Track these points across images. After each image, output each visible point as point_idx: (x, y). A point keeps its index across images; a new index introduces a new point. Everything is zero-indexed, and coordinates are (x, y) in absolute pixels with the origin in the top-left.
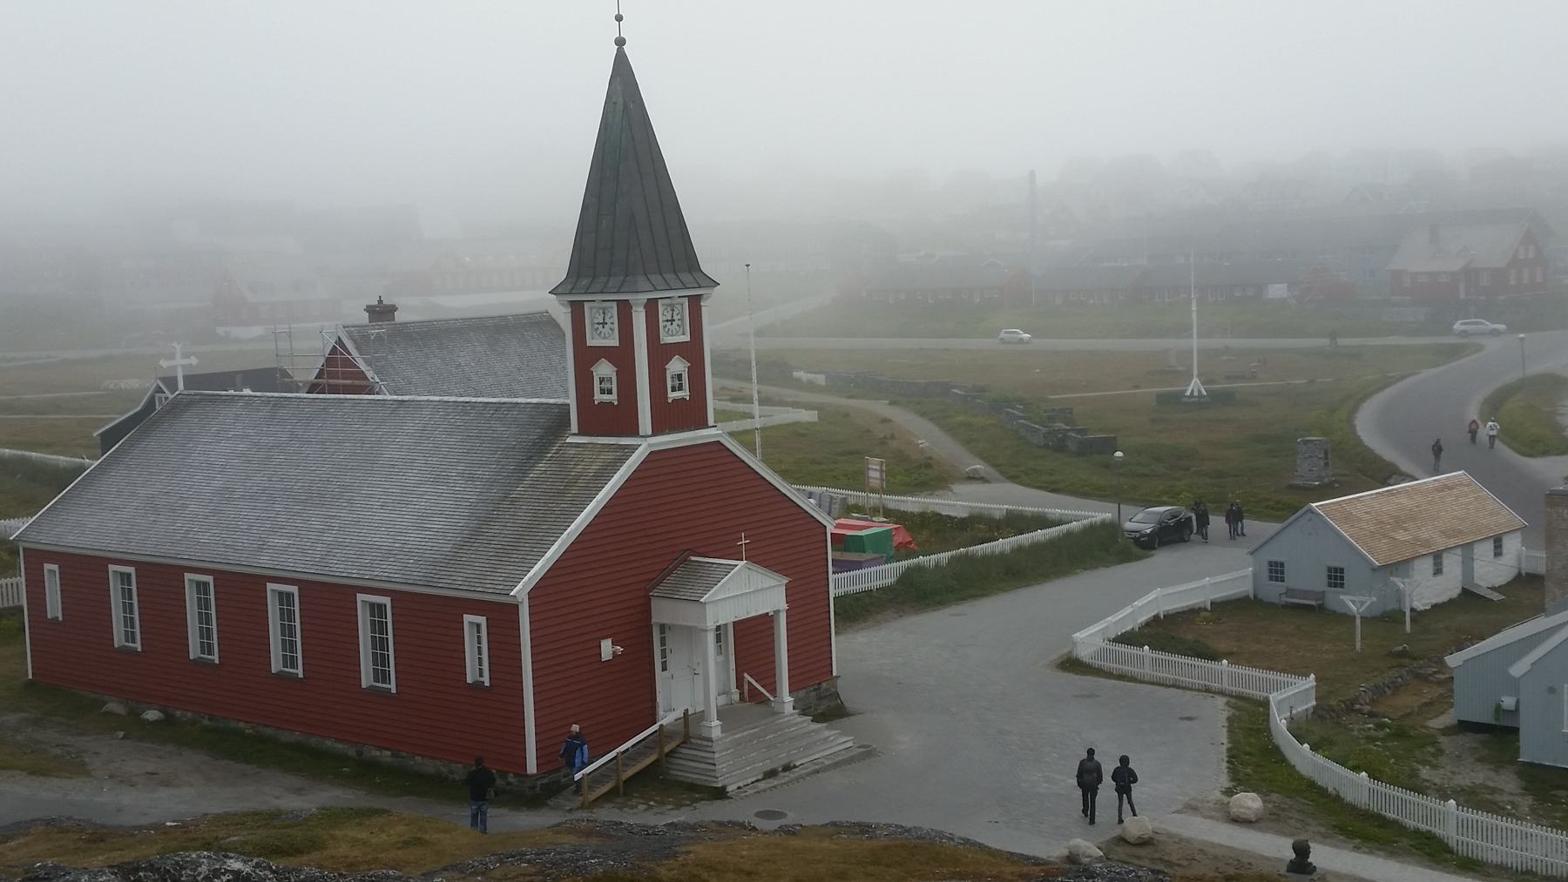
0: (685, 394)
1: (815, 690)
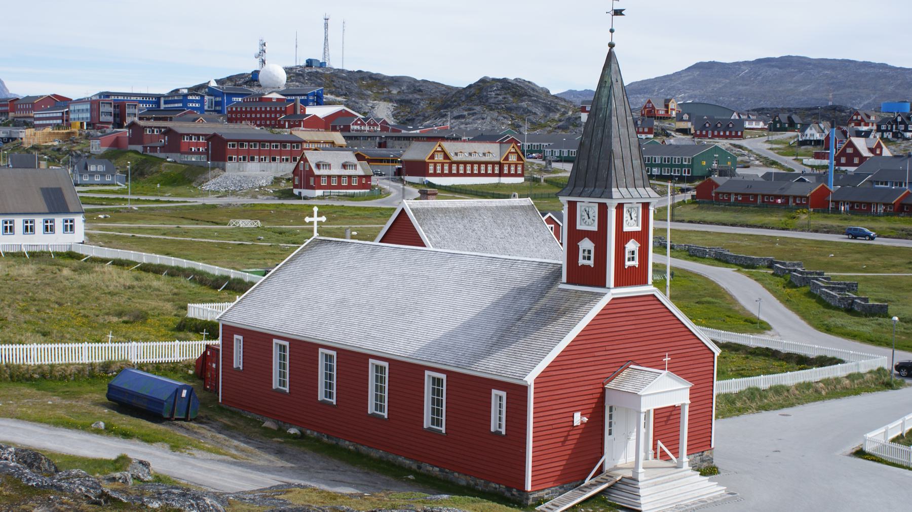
0: (635, 263)
1: (699, 456)
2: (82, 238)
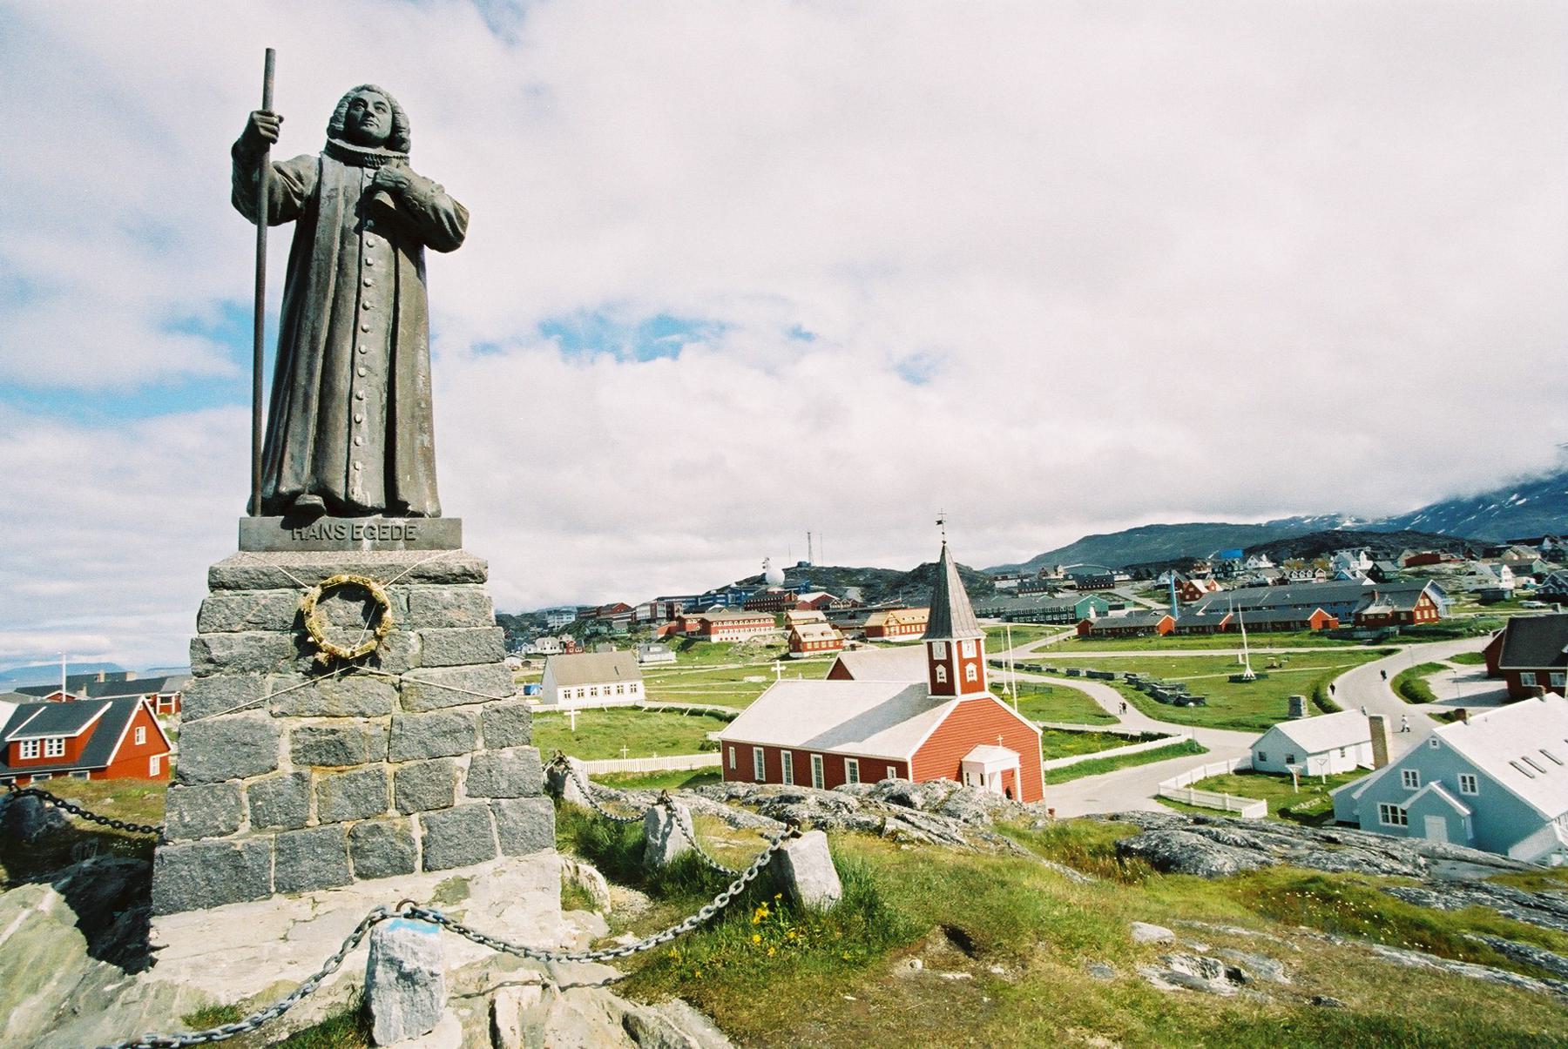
2: (643, 697)
